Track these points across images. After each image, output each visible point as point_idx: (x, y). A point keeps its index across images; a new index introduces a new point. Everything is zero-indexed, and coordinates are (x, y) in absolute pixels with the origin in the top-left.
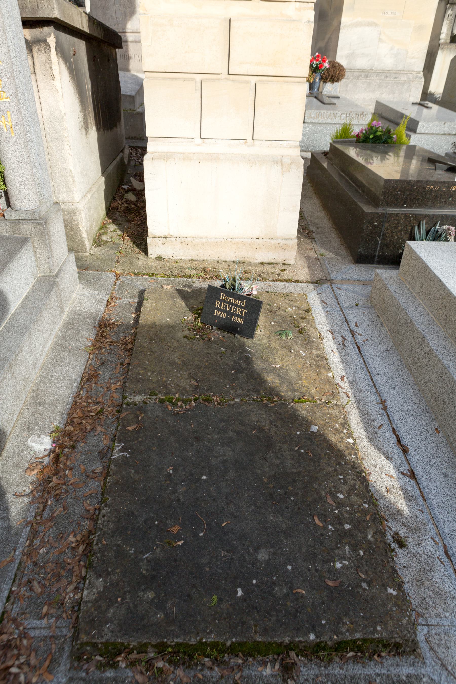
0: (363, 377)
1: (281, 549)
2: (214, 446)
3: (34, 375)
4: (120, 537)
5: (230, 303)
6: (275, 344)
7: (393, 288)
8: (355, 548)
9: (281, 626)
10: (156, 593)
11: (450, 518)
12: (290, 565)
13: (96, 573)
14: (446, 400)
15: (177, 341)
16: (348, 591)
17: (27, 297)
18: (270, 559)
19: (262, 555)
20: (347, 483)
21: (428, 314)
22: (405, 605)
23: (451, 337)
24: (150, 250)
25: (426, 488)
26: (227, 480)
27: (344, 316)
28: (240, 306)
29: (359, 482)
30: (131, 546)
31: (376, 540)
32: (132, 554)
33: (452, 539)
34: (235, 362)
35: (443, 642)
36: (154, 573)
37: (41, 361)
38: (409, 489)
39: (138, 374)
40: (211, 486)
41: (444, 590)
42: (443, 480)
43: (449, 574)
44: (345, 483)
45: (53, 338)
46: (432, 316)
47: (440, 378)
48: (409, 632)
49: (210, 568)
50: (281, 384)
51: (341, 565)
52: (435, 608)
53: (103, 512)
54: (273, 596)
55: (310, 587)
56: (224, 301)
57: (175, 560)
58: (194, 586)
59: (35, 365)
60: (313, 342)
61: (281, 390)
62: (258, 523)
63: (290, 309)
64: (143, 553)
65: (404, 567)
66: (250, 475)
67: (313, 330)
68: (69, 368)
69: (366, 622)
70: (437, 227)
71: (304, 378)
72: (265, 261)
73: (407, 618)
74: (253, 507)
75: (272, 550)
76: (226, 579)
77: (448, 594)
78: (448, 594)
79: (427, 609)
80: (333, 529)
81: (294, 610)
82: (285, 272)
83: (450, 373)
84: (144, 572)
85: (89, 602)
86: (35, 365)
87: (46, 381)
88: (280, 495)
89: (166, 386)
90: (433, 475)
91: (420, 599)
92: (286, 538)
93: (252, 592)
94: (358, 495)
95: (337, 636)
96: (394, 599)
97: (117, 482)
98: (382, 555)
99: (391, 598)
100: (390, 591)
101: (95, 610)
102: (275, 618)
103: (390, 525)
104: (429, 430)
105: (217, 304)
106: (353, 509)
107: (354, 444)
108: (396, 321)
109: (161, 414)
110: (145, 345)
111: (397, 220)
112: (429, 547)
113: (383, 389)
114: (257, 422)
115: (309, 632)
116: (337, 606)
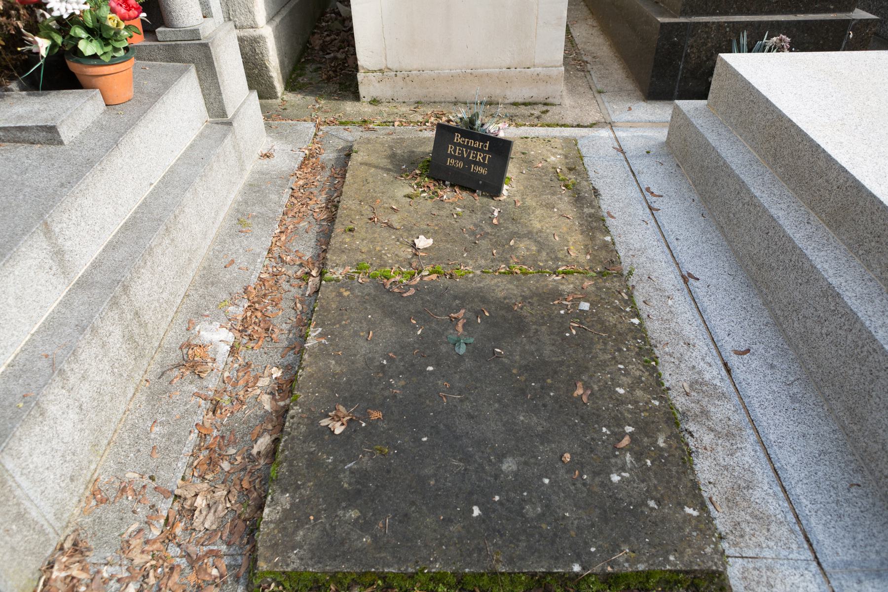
0: (655, 243)
1: (536, 457)
2: (444, 330)
3: (204, 248)
4: (314, 442)
5: (467, 147)
6: (530, 202)
7: (699, 122)
8: (639, 456)
9: (533, 554)
10: (361, 512)
11: (777, 422)
12: (547, 477)
13: (280, 487)
14: (773, 265)
15: (397, 201)
16: (630, 511)
17: (192, 146)
18: (519, 470)
19: (509, 465)
20: (629, 374)
21: (749, 152)
22: (710, 529)
23: (782, 179)
24: (362, 90)
25: (744, 383)
26: (461, 372)
27: (630, 167)
28: (481, 150)
29: (647, 373)
30: (329, 454)
31: (670, 446)
32: (330, 464)
33: (780, 448)
34: (475, 225)
35: (764, 579)
36: (359, 487)
37: (215, 231)
38: (718, 384)
39: (343, 243)
40: (439, 379)
41: (767, 513)
42: (769, 372)
43: (774, 493)
44: (627, 373)
45: (230, 202)
46: (755, 154)
47: (765, 236)
48: (716, 564)
49: (436, 481)
50: (539, 251)
51: (619, 478)
52: (753, 535)
53: (291, 412)
54: (523, 516)
55: (575, 506)
56: (459, 144)
57: (388, 472)
58: (413, 503)
59: (205, 235)
60: (585, 197)
61: (539, 258)
62: (504, 425)
63: (553, 158)
64: (344, 462)
65: (710, 483)
66: (493, 365)
67: (585, 183)
68: (252, 239)
69: (653, 550)
70: (765, 40)
71: (571, 243)
72: (520, 100)
73: (712, 546)
74: (497, 405)
75: (523, 459)
76: (457, 496)
77: (774, 518)
78: (774, 518)
79: (742, 536)
80: (608, 433)
81: (551, 534)
82: (548, 114)
83: (780, 226)
84: (346, 485)
85: (271, 522)
86: (205, 235)
87: (221, 255)
88: (535, 389)
89: (381, 258)
90: (753, 366)
91: (733, 524)
92: (542, 444)
93: (494, 511)
94: (644, 390)
95: (612, 567)
96: (694, 522)
97: (311, 375)
98: (679, 465)
99: (690, 520)
100: (689, 511)
101: (279, 532)
102: (524, 544)
103: (691, 429)
104: (749, 309)
105: (450, 150)
106: (637, 407)
107: (640, 324)
108: (702, 167)
109: (372, 291)
110: (353, 207)
111: (706, 33)
112: (747, 459)
113: (683, 258)
114: (505, 298)
115: (573, 562)
116: (612, 530)
